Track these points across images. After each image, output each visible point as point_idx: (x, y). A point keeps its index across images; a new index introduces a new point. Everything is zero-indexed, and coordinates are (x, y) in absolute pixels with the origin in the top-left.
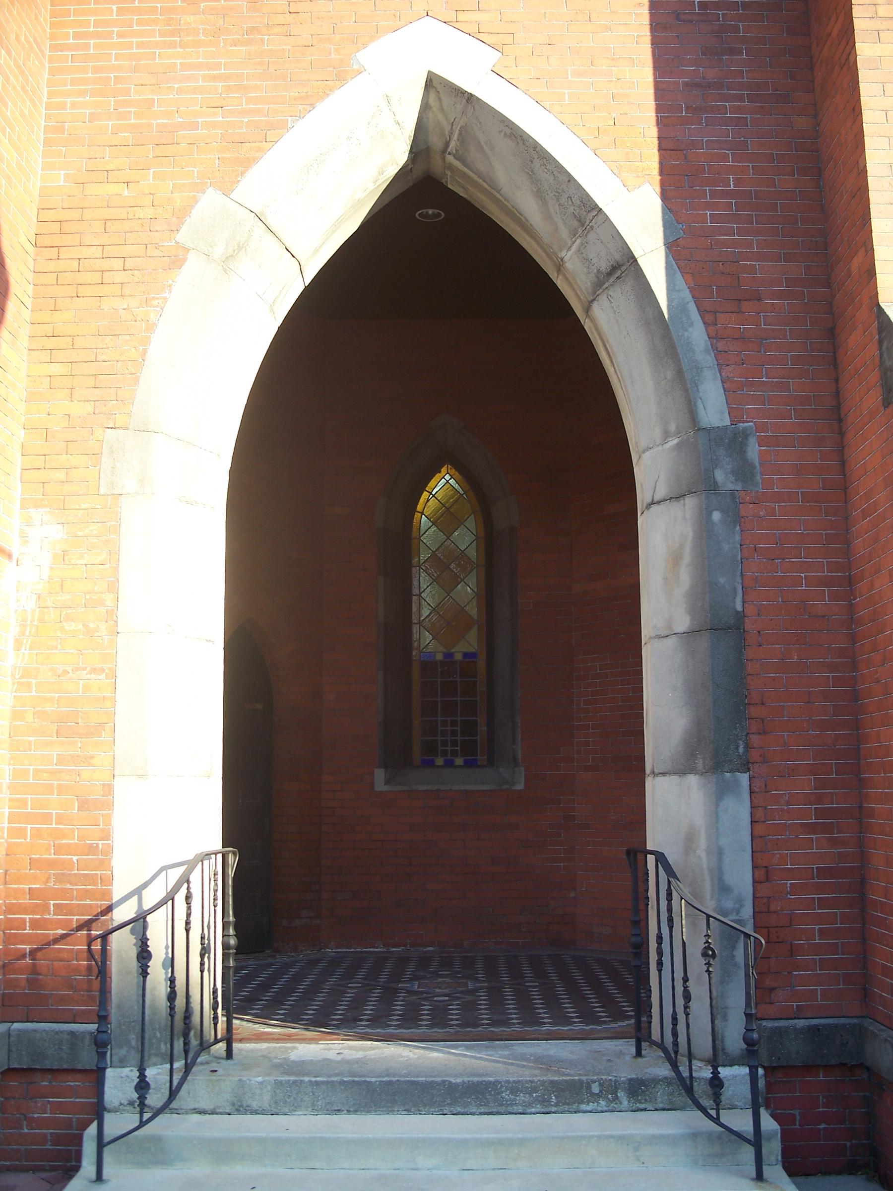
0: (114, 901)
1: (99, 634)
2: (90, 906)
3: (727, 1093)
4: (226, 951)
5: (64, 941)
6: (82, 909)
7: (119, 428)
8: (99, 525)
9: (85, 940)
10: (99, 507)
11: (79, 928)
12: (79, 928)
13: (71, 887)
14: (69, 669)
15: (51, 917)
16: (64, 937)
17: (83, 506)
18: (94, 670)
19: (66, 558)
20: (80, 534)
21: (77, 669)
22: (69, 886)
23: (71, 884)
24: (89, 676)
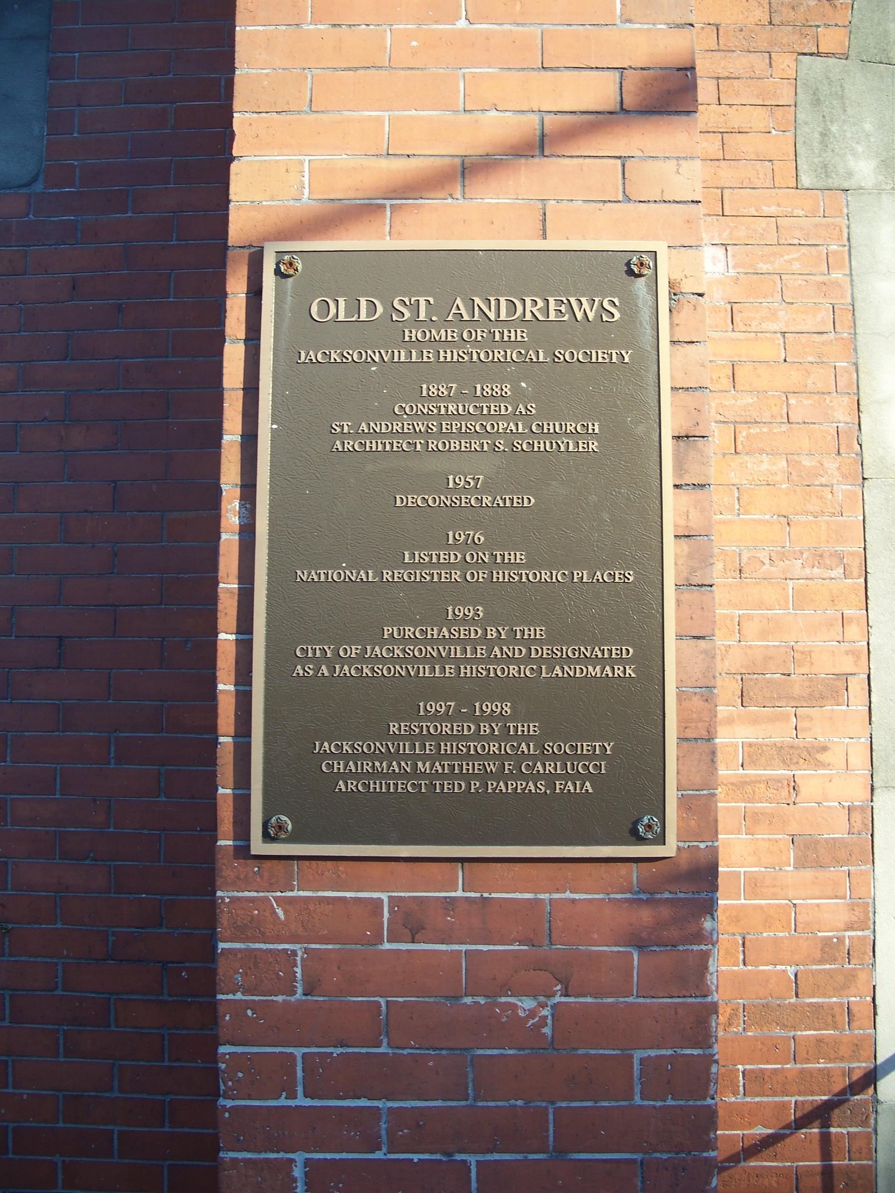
0: (880, 1060)
1: (823, 480)
2: (827, 1074)
3: (736, 687)
4: (247, 688)
5: (770, 1151)
6: (805, 1080)
7: (827, 55)
8: (804, 250)
9: (816, 1147)
10: (801, 213)
11: (803, 1122)
12: (803, 1122)
13: (783, 1033)
14: (764, 556)
15: (740, 1098)
16: (768, 1142)
17: (766, 210)
18: (819, 557)
19: (737, 319)
20: (763, 267)
21: (783, 556)
22: (778, 1031)
23: (784, 1027)
24: (808, 571)
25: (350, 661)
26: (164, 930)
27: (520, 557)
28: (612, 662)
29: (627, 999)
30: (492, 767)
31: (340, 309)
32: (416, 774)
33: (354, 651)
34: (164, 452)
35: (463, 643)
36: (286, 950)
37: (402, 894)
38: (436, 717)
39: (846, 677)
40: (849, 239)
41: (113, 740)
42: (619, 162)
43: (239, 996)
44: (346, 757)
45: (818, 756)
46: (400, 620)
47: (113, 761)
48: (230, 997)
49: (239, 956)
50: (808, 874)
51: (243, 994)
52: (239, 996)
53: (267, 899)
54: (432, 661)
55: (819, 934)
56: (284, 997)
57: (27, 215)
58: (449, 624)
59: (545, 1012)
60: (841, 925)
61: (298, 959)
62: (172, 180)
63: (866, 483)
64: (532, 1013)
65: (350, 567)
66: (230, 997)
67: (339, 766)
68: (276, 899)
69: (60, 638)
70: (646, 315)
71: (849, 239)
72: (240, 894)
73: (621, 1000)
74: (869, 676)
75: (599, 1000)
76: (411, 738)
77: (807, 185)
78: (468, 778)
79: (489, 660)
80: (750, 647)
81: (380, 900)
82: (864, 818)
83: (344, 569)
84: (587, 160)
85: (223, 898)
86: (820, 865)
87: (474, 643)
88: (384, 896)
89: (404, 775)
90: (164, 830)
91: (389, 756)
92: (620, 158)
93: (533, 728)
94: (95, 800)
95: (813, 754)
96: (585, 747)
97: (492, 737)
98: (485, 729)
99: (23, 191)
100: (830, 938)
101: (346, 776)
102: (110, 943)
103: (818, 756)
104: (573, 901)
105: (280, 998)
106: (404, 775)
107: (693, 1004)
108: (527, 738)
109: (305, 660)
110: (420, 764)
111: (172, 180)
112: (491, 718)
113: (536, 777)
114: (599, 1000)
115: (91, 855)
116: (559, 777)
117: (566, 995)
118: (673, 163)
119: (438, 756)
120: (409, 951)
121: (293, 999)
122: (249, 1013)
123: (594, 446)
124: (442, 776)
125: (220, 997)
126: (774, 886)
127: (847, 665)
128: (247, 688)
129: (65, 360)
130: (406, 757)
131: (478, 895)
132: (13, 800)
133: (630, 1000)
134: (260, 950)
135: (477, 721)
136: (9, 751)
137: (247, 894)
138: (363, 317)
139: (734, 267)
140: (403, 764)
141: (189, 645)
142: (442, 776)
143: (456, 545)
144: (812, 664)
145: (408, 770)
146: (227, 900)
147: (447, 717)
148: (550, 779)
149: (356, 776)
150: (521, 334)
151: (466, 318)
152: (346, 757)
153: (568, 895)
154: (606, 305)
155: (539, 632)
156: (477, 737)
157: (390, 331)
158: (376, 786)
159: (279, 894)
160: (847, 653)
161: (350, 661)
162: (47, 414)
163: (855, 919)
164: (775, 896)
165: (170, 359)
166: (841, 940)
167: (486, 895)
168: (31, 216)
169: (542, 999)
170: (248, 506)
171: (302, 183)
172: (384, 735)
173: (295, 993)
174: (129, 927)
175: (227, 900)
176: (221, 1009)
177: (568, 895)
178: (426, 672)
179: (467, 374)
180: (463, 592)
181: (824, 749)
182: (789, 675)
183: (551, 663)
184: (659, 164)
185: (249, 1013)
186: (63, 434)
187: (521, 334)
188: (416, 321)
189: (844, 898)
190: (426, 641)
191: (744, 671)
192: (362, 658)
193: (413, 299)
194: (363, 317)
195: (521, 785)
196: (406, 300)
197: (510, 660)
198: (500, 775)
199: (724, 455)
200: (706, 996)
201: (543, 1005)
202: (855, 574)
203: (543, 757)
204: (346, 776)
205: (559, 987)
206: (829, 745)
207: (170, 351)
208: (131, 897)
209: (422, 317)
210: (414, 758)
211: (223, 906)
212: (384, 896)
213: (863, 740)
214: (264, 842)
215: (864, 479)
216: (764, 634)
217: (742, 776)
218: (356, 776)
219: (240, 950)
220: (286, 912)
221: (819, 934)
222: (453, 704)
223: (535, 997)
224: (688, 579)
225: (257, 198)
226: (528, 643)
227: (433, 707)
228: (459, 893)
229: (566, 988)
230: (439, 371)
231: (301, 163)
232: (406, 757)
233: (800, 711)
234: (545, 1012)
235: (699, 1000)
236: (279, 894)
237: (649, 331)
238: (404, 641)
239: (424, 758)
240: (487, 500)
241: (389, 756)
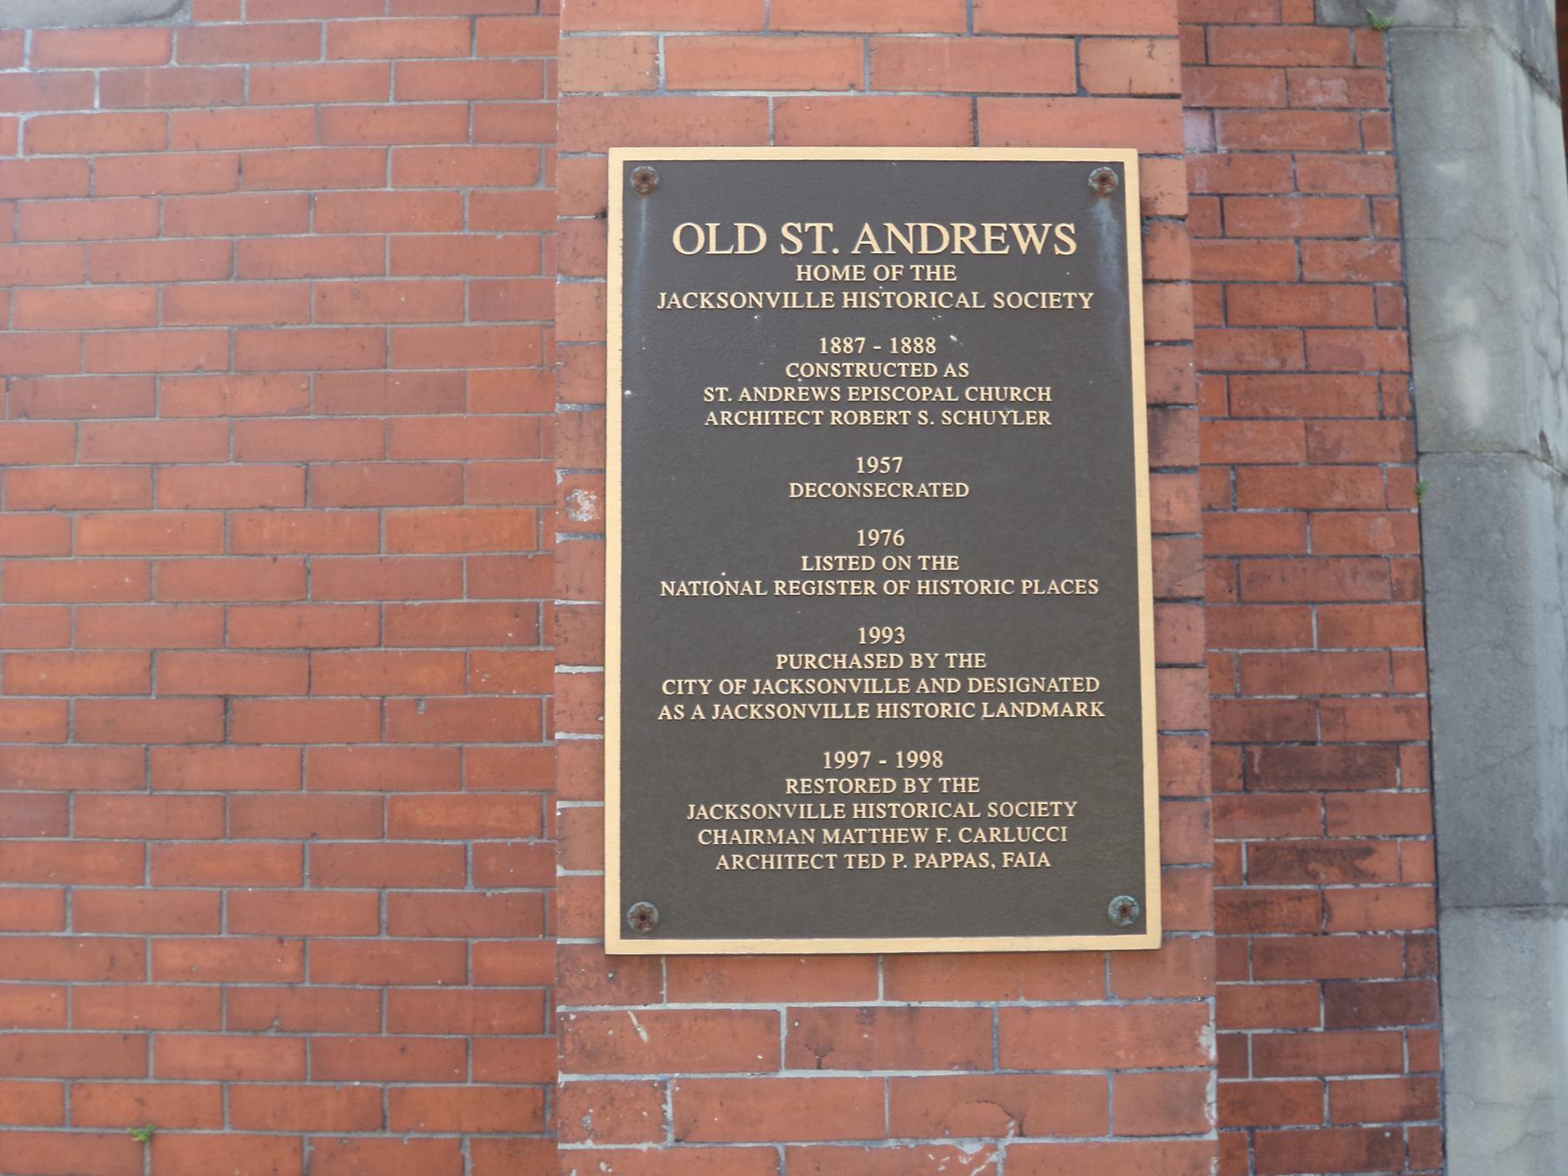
25: (732, 700)
26: (388, 1134)
27: (951, 562)
28: (1072, 698)
29: (1100, 1139)
30: (919, 835)
31: (707, 238)
32: (819, 846)
33: (737, 686)
34: (381, 418)
35: (880, 674)
36: (651, 1082)
37: (805, 1005)
38: (845, 772)
39: (1395, 746)
40: (1392, 101)
41: (307, 850)
42: (1072, 42)
43: (589, 1144)
44: (730, 825)
45: (1358, 863)
46: (798, 645)
47: (308, 881)
48: (578, 1146)
49: (589, 1091)
50: (1346, 1038)
51: (595, 1141)
52: (589, 1144)
53: (625, 1015)
54: (839, 698)
55: (1366, 1126)
56: (651, 1145)
57: (168, 60)
58: (862, 650)
59: (993, 1158)
60: (1397, 1113)
61: (668, 1093)
62: (387, 10)
63: (1422, 460)
64: (978, 1159)
65: (731, 578)
66: (578, 1146)
67: (720, 837)
68: (638, 1014)
69: (225, 699)
70: (1109, 246)
71: (1392, 101)
72: (591, 1009)
73: (1093, 1140)
74: (1430, 743)
75: (1063, 1141)
76: (814, 798)
77: (1329, 20)
78: (888, 849)
79: (911, 697)
80: (1257, 703)
81: (776, 1013)
82: (1425, 950)
83: (723, 580)
84: (1030, 40)
85: (566, 1015)
86: (1362, 1023)
87: (894, 674)
88: (782, 1008)
89: (807, 848)
90: (388, 984)
91: (784, 823)
92: (1071, 37)
93: (970, 784)
94: (281, 941)
95: (1352, 860)
96: (1039, 808)
97: (917, 797)
98: (909, 785)
99: (159, 24)
100: (1380, 1132)
101: (729, 850)
102: (306, 1155)
103: (1358, 863)
104: (1028, 1010)
105: (644, 1147)
106: (807, 848)
107: (1185, 1144)
108: (964, 798)
109: (672, 701)
110: (826, 832)
111: (387, 10)
112: (918, 772)
113: (976, 849)
114: (1063, 1141)
115: (276, 1023)
116: (1008, 847)
117: (1021, 1135)
118: (1144, 43)
119: (848, 823)
120: (814, 1080)
121: (659, 1147)
122: (603, 1166)
123: (1044, 418)
124: (855, 848)
125: (561, 1146)
126: (1297, 1056)
127: (1397, 728)
128: (597, 737)
129: (228, 278)
130: (808, 824)
131: (903, 1004)
132: (156, 942)
133: (1106, 1139)
134: (618, 1082)
135: (899, 775)
136: (148, 868)
137: (599, 1008)
138: (741, 250)
139: (1225, 142)
140: (804, 832)
141: (423, 706)
142: (855, 848)
143: (866, 550)
144: (1346, 726)
145: (811, 840)
146: (573, 1017)
147: (858, 772)
148: (996, 850)
149: (744, 850)
150: (946, 272)
151: (877, 250)
152: (730, 825)
153: (1023, 1002)
154: (1059, 234)
155: (977, 659)
156: (899, 796)
157: (772, 269)
158: (769, 862)
159: (642, 1007)
160: (1398, 709)
161: (732, 700)
162: (202, 360)
163: (1416, 1102)
164: (1298, 1071)
165: (388, 279)
166: (1397, 1134)
167: (914, 1004)
168: (174, 63)
169: (987, 1140)
170: (593, 497)
171: (657, 69)
172: (778, 795)
173: (664, 1138)
174: (335, 1130)
175: (573, 1017)
176: (565, 1163)
177: (1023, 1002)
178: (830, 711)
179: (880, 328)
180: (881, 609)
181: (1367, 852)
182: (1313, 743)
183: (995, 699)
184: (1125, 45)
185: (603, 1166)
186: (227, 391)
187: (946, 272)
188: (807, 257)
189: (1400, 1070)
190: (831, 674)
191: (1246, 738)
192: (747, 696)
193: (808, 225)
194: (741, 250)
195: (958, 858)
196: (798, 226)
197: (939, 697)
198: (930, 846)
199: (1213, 420)
200: (1201, 1133)
201: (993, 1148)
202: (1408, 593)
203: (986, 823)
204: (729, 850)
205: (1012, 1124)
206: (1373, 845)
207: (388, 266)
208: (338, 1085)
209: (819, 250)
210: (819, 824)
211: (566, 1026)
212: (782, 1008)
213: (1423, 838)
214: (623, 937)
215: (1419, 454)
216: (1275, 684)
217: (1247, 892)
218: (744, 850)
219: (589, 1084)
220: (650, 1031)
221: (1366, 1126)
222: (868, 753)
223: (980, 1138)
224: (1170, 590)
225: (596, 89)
226: (962, 674)
227: (844, 758)
228: (880, 1002)
229: (1020, 1126)
230: (842, 322)
231: (655, 40)
232: (808, 824)
233: (1330, 797)
234: (993, 1158)
235: (1195, 1138)
236: (642, 1007)
237: (1114, 263)
238: (803, 673)
239: (831, 825)
240: (907, 490)
241: (784, 823)
